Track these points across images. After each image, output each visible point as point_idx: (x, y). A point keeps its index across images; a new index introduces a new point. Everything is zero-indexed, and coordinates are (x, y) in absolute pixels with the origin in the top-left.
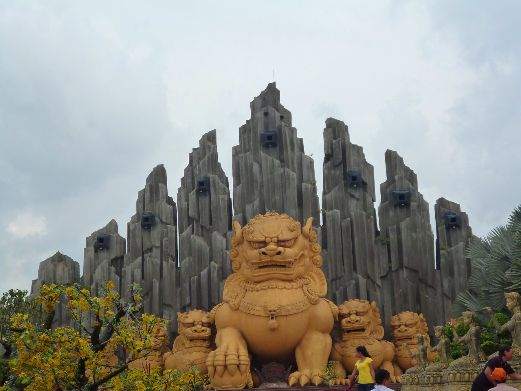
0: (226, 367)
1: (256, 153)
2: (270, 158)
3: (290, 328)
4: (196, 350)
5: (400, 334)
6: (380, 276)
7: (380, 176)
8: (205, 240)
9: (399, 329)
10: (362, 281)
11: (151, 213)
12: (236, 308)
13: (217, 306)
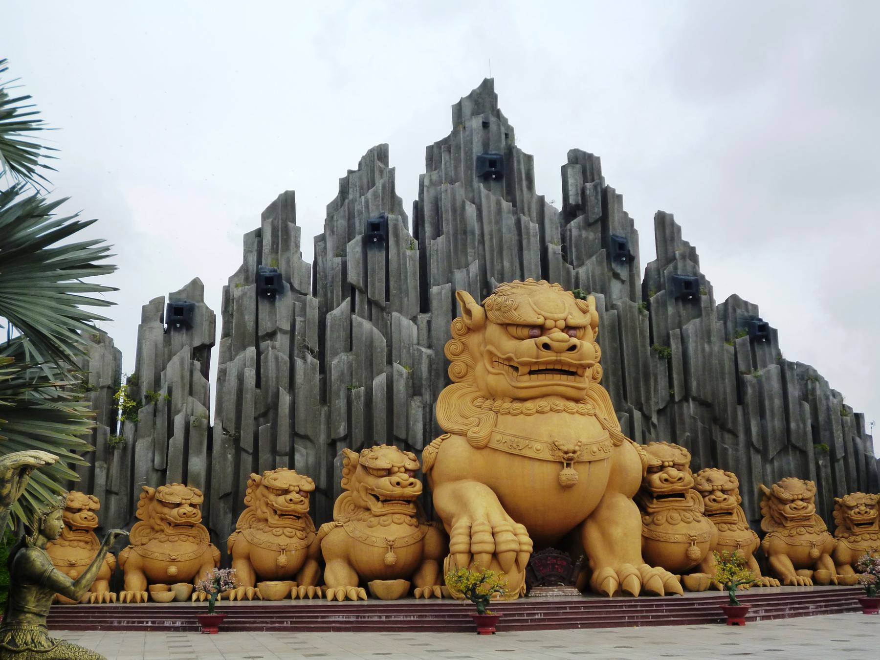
1: (469, 184)
2: (493, 198)
3: (589, 480)
6: (657, 408)
11: (275, 271)
12: (482, 444)
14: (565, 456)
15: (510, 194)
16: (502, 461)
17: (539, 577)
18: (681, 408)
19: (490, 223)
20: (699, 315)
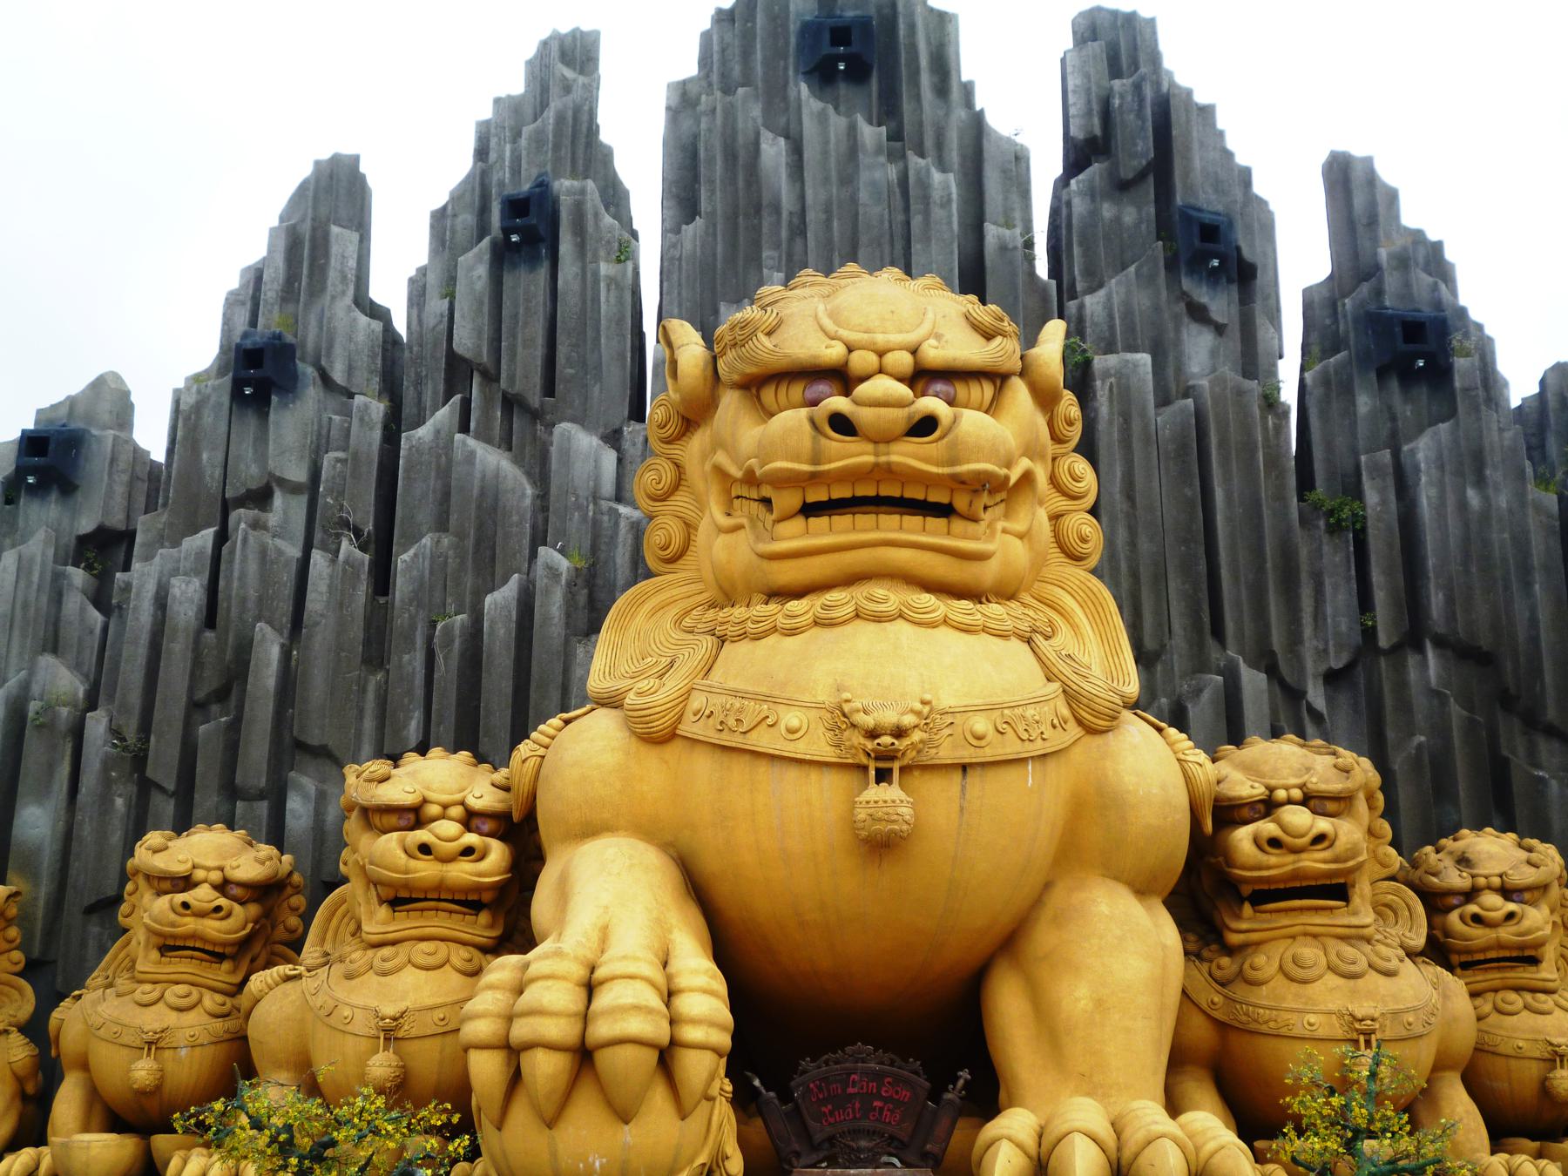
0: (584, 1055)
2: (837, 122)
3: (980, 834)
4: (420, 960)
5: (1480, 935)
6: (1323, 668)
7: (1301, 258)
8: (518, 461)
9: (1473, 908)
10: (1253, 681)
12: (661, 724)
13: (555, 721)
14: (870, 745)
15: (889, 110)
16: (703, 766)
17: (818, 1137)
18: (1400, 669)
19: (826, 180)
20: (1452, 413)
